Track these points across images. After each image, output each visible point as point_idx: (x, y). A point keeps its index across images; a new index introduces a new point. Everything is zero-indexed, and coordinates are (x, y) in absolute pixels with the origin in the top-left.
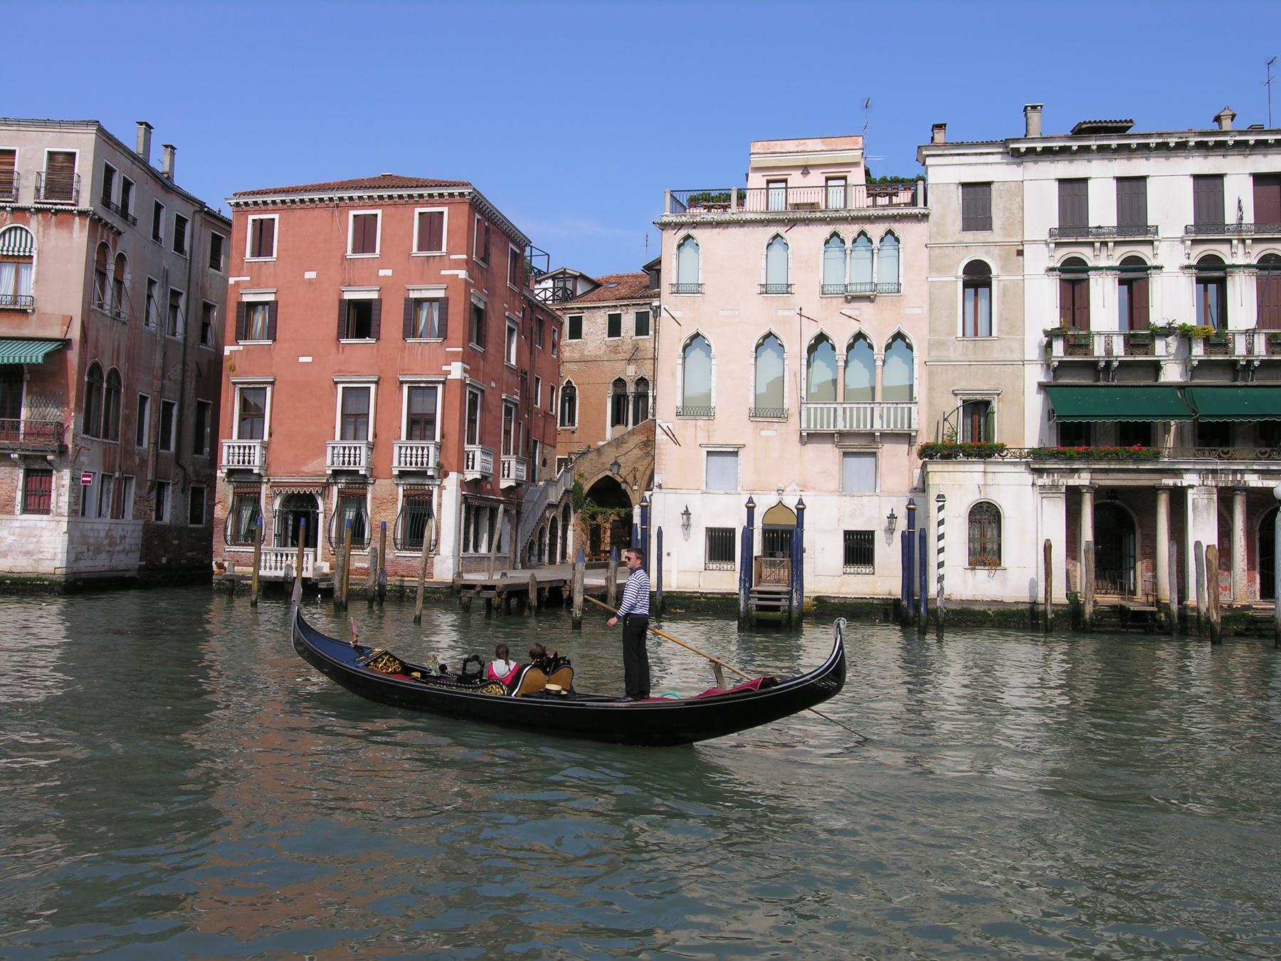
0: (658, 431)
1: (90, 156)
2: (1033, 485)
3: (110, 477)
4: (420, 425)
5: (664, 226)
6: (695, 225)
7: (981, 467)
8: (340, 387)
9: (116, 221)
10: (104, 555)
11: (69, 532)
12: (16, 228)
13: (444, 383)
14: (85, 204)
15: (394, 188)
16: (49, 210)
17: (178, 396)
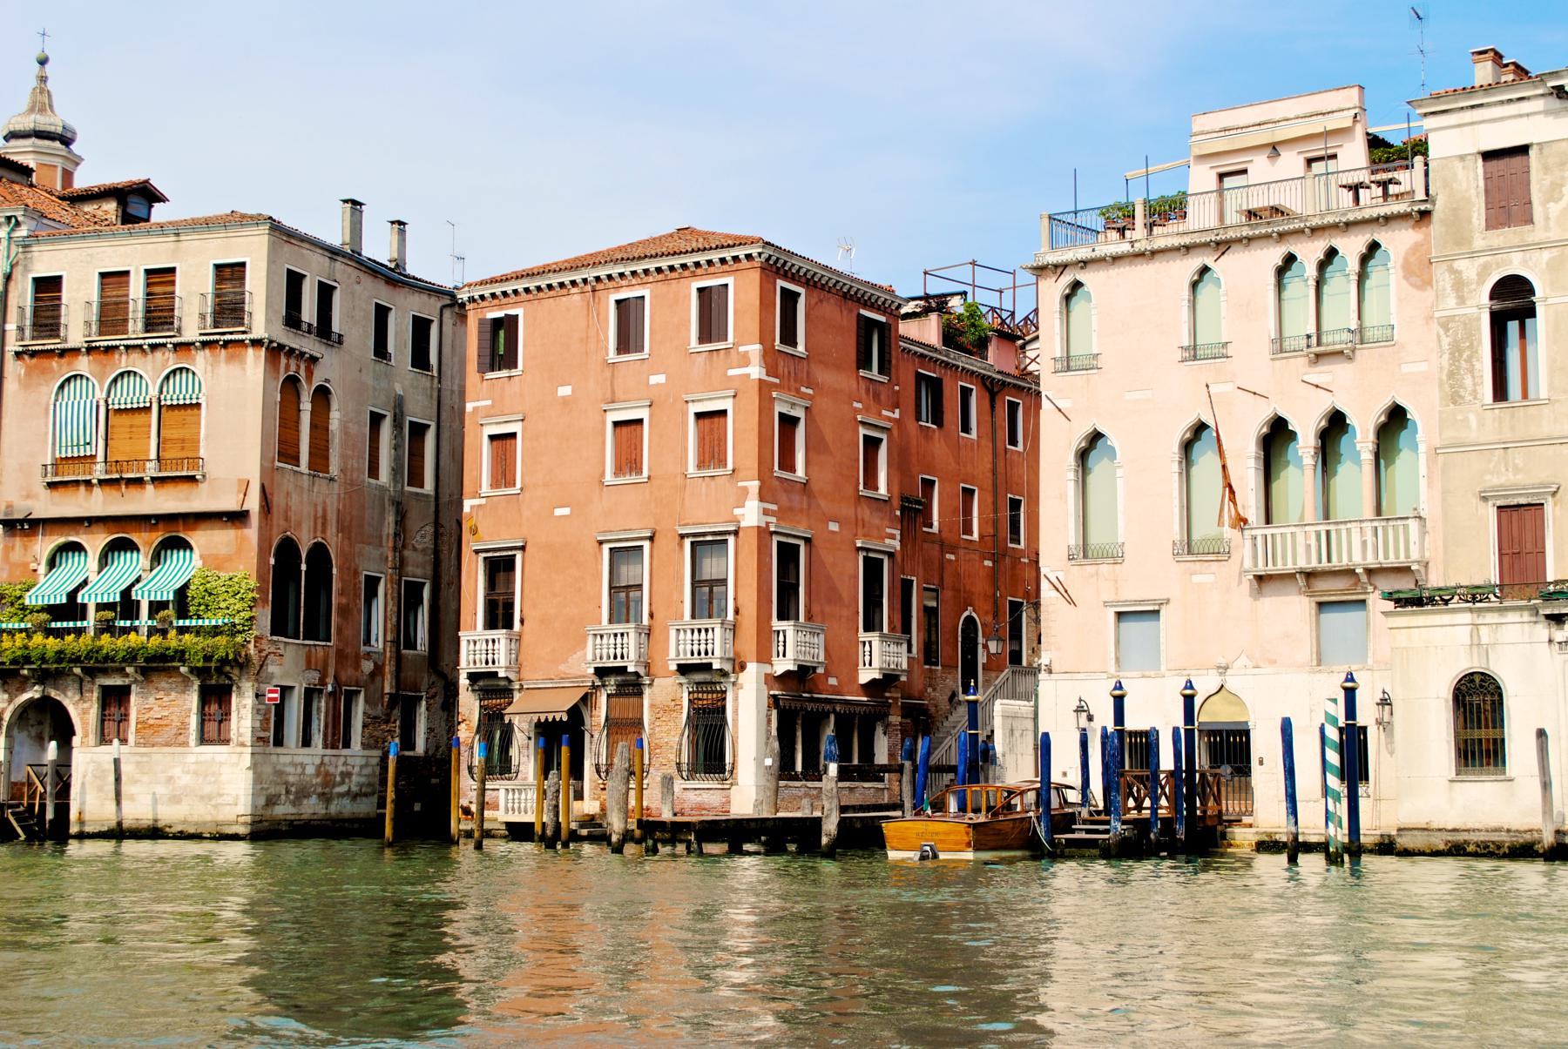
0: (1044, 585)
1: (263, 265)
2: (1550, 641)
3: (320, 691)
4: (706, 596)
5: (1040, 270)
6: (1084, 264)
7: (1467, 617)
8: (606, 547)
9: (310, 345)
10: (314, 799)
11: (254, 766)
12: (181, 369)
13: (736, 533)
14: (259, 331)
15: (678, 253)
16: (217, 342)
17: (429, 570)
